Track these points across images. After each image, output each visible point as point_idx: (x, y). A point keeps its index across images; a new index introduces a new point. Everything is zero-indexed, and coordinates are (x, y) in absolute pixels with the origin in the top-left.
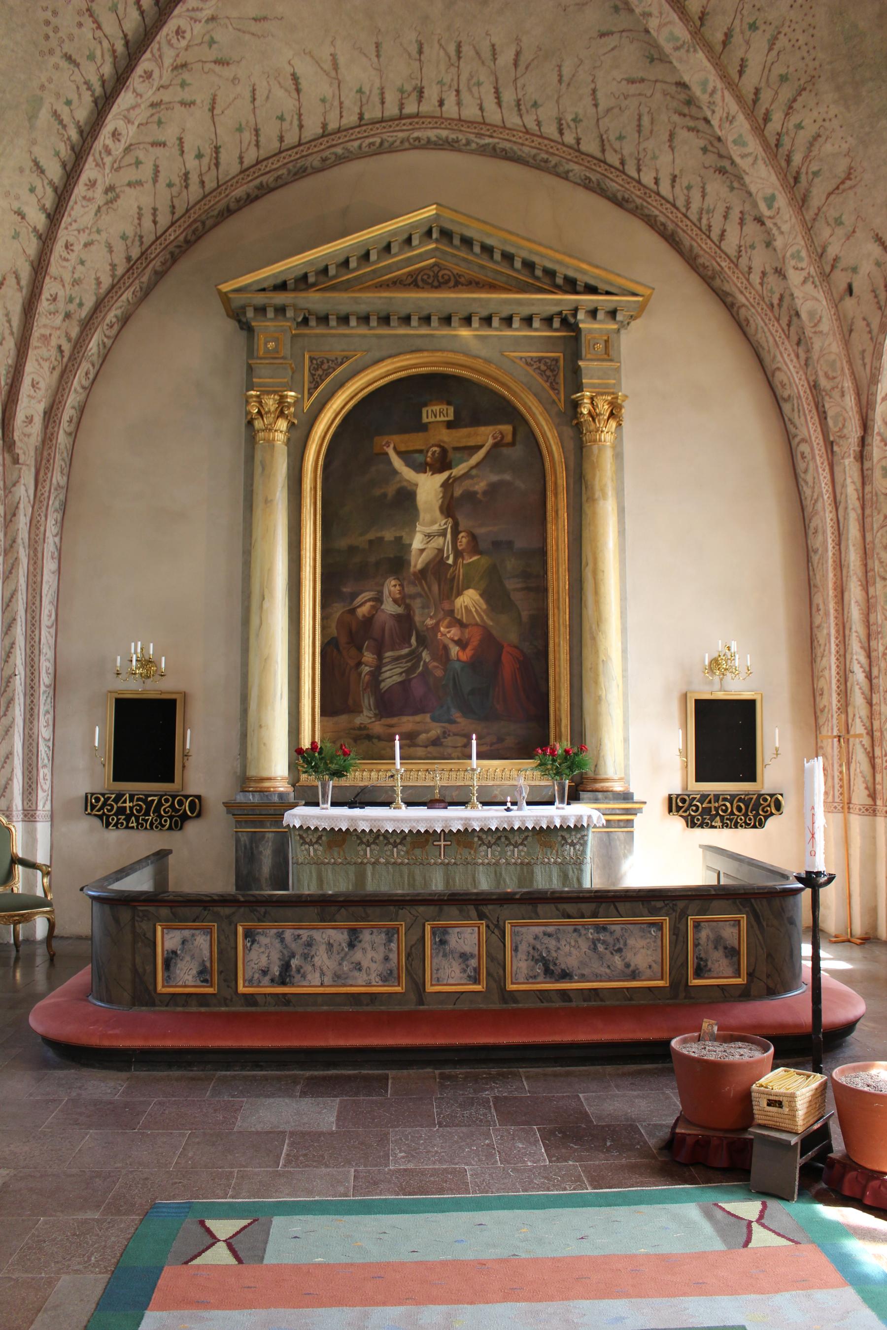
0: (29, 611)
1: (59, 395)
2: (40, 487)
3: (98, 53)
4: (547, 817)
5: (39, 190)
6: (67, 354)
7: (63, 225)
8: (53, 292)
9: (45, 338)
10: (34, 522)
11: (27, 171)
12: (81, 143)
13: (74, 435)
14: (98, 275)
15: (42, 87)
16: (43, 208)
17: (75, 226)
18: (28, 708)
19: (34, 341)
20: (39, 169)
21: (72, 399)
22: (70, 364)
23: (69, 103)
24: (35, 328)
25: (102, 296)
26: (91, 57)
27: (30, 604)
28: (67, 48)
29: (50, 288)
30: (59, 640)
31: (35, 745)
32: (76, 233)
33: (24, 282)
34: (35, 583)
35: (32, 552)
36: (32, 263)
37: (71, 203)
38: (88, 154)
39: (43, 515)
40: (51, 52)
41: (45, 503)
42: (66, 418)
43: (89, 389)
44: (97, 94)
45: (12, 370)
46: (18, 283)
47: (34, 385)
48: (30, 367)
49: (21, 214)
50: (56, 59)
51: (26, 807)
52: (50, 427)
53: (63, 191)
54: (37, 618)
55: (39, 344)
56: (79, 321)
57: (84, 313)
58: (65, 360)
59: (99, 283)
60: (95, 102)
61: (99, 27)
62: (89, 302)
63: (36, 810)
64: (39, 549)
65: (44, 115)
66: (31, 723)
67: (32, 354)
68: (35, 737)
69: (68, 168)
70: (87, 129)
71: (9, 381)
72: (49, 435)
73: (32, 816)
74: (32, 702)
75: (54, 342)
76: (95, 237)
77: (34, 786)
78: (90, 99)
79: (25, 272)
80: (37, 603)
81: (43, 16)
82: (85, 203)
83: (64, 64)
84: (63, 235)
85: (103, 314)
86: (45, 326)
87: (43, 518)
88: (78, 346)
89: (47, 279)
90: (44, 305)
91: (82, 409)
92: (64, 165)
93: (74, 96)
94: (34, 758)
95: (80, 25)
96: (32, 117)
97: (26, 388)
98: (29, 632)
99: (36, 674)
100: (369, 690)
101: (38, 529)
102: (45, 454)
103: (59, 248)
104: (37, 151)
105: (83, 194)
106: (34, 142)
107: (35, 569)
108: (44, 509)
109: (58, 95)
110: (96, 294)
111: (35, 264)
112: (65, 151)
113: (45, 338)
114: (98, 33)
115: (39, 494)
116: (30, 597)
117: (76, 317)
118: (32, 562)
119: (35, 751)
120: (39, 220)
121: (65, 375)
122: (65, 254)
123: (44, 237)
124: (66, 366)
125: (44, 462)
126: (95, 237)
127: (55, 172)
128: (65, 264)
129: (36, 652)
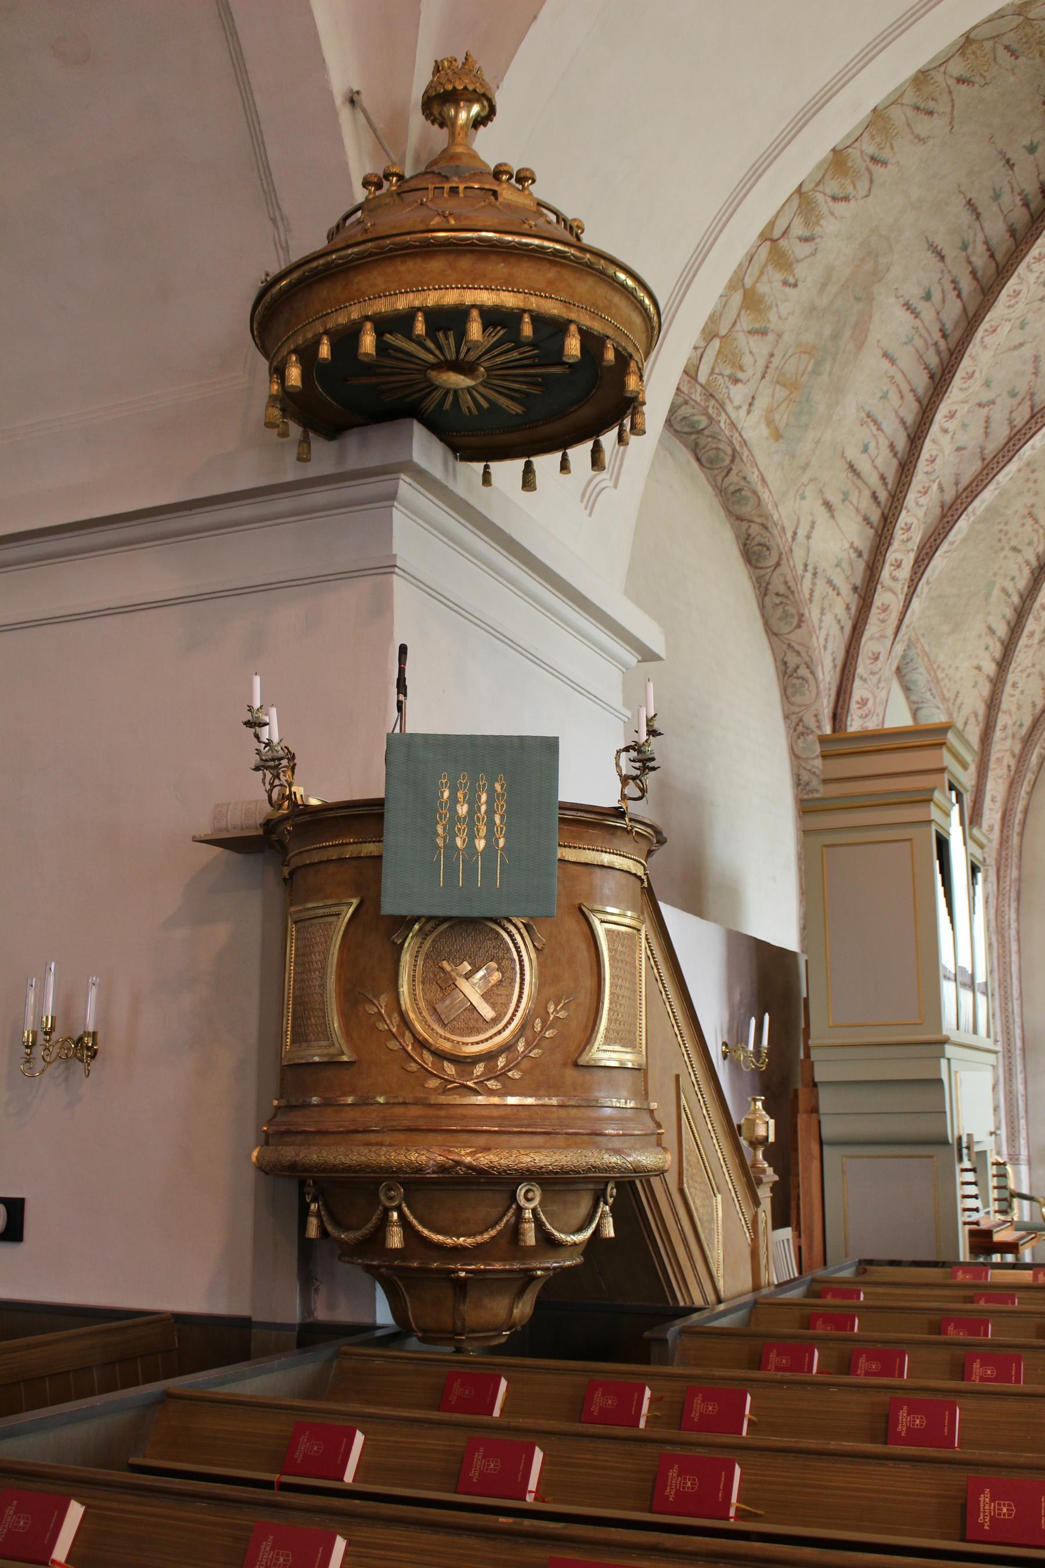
0: (1002, 987)
1: (1010, 803)
2: (1001, 883)
3: (1035, 539)
4: (267, 407)
5: (991, 648)
6: (1013, 768)
7: (1011, 670)
8: (1004, 723)
9: (999, 760)
10: (999, 912)
11: (984, 636)
12: (1021, 604)
13: (1021, 834)
14: (1034, 699)
15: (995, 574)
16: (994, 659)
17: (1019, 669)
18: (1007, 1068)
19: (992, 765)
20: (991, 631)
21: (1020, 806)
22: (1016, 776)
23: (1013, 579)
24: (992, 754)
25: (1038, 716)
26: (1030, 543)
27: (1002, 981)
28: (1013, 543)
29: (1002, 719)
30: (1024, 1010)
31: (1015, 1099)
32: (1019, 674)
33: (981, 718)
34: (1005, 963)
35: (1000, 938)
36: (986, 702)
37: (1016, 653)
38: (1029, 613)
39: (1006, 905)
40: (1002, 549)
41: (1007, 895)
42: (1017, 821)
43: (1030, 794)
44: (1034, 567)
45: (975, 789)
46: (977, 720)
47: (993, 800)
48: (990, 786)
49: (979, 668)
50: (1007, 552)
51: (1011, 1153)
52: (1005, 831)
53: (1008, 644)
54: (1009, 992)
55: (995, 766)
56: (1021, 739)
57: (1023, 731)
58: (1012, 773)
59: (1034, 705)
60: (1032, 573)
61: (1037, 522)
62: (1028, 722)
63: (1020, 1154)
64: (1006, 934)
65: (996, 592)
66: (1011, 1081)
67: (991, 775)
68: (1014, 1092)
69: (1012, 624)
70: (1026, 593)
71: (973, 798)
72: (1004, 838)
73: (1017, 1160)
74: (1010, 1063)
75: (1005, 763)
76: (1032, 670)
77: (1016, 1134)
78: (1029, 571)
79: (981, 710)
80: (1008, 979)
81: (997, 528)
82: (1026, 650)
83: (1011, 554)
84: (1011, 678)
85: (1040, 731)
86: (999, 751)
87: (1007, 908)
88: (1022, 760)
89: (1000, 714)
90: (998, 734)
91: (1026, 811)
92: (1009, 623)
93: (1016, 573)
94: (1015, 1110)
95: (1023, 525)
96: (988, 596)
97: (987, 803)
98: (1003, 1005)
99: (1012, 1039)
100: (311, 435)
101: (1003, 917)
102: (1004, 854)
103: (1008, 689)
104: (991, 619)
105: (1025, 643)
106: (988, 614)
107: (1004, 951)
108: (1007, 900)
109: (1005, 576)
110: (1033, 715)
111: (989, 702)
112: (1009, 613)
113: (999, 760)
114: (1036, 526)
115: (1001, 888)
116: (1002, 976)
117: (1018, 736)
118: (1000, 946)
119: (1015, 1105)
120: (990, 668)
121: (1013, 786)
122: (1012, 692)
123: (994, 681)
124: (1014, 778)
125: (1003, 861)
126: (1032, 670)
127: (1002, 630)
128: (1012, 699)
129: (1011, 1021)
